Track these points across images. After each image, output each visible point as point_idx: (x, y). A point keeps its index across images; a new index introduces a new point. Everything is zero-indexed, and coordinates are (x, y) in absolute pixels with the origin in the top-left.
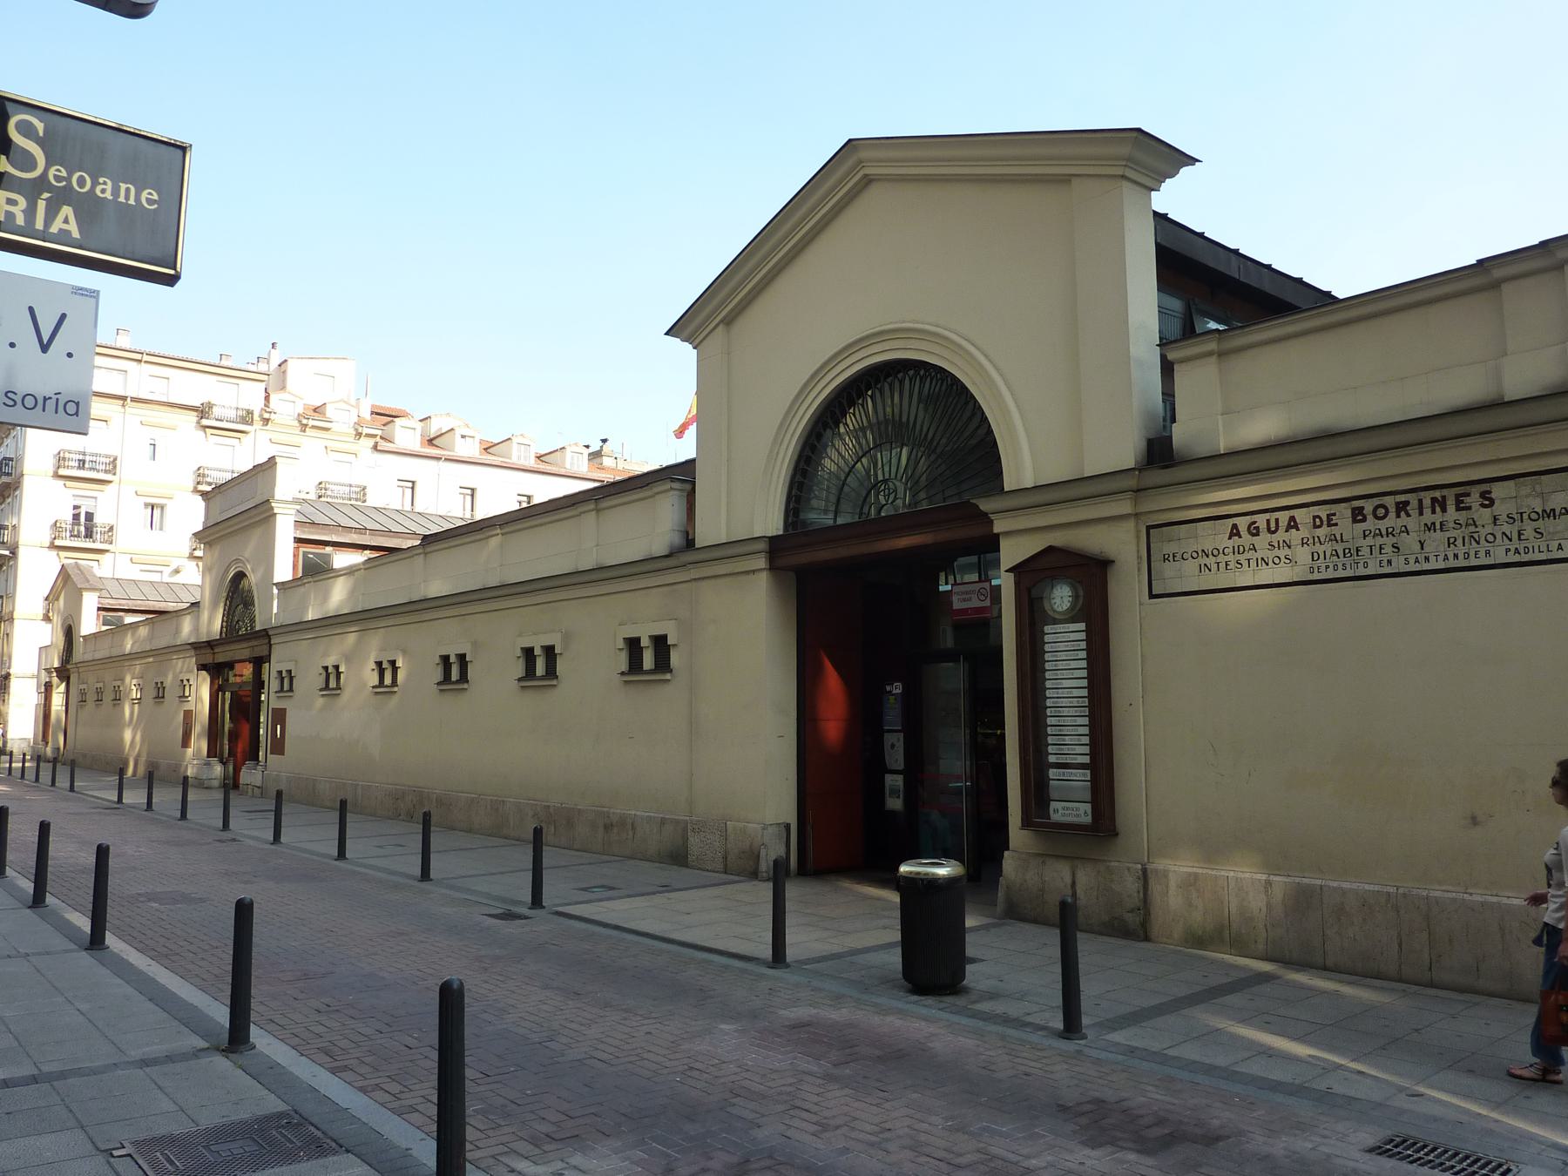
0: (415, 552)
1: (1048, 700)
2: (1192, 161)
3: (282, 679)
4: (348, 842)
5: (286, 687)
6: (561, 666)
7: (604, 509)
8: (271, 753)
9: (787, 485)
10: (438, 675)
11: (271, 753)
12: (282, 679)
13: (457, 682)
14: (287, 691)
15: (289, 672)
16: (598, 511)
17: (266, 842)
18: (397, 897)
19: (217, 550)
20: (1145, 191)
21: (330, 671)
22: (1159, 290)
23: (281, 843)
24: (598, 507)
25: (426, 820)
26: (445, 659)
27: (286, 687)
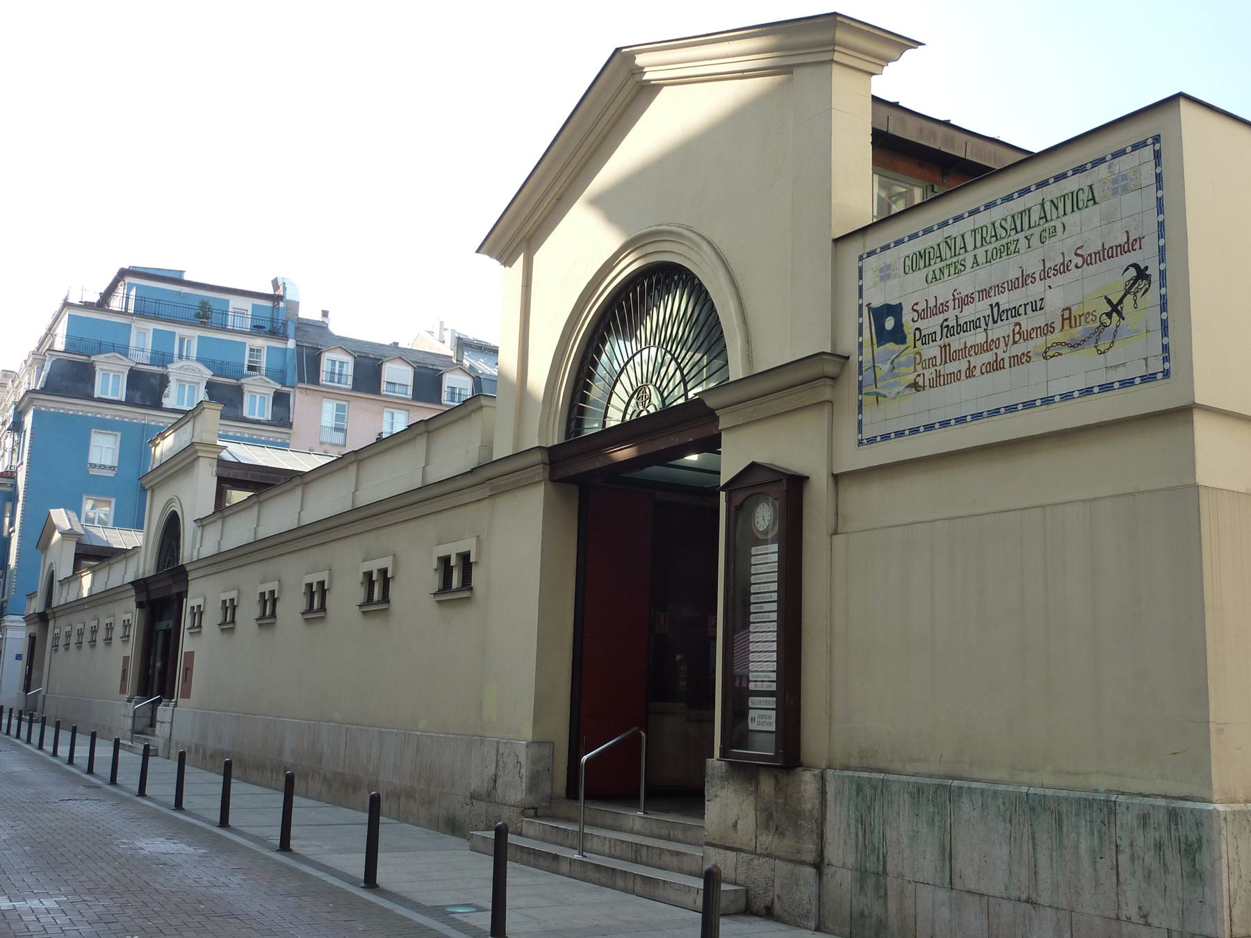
0: (470, 408)
1: (752, 606)
2: (905, 43)
3: (312, 594)
4: (381, 857)
5: (377, 595)
6: (477, 576)
7: (227, 516)
8: (181, 697)
9: (571, 388)
10: (435, 582)
11: (181, 697)
12: (312, 594)
13: (458, 590)
14: (378, 603)
15: (322, 583)
16: (109, 565)
17: (166, 805)
18: (100, 809)
19: (220, 469)
20: (865, 76)
21: (314, 589)
22: (876, 162)
23: (117, 784)
24: (429, 429)
25: (290, 782)
26: (445, 561)
27: (377, 595)
